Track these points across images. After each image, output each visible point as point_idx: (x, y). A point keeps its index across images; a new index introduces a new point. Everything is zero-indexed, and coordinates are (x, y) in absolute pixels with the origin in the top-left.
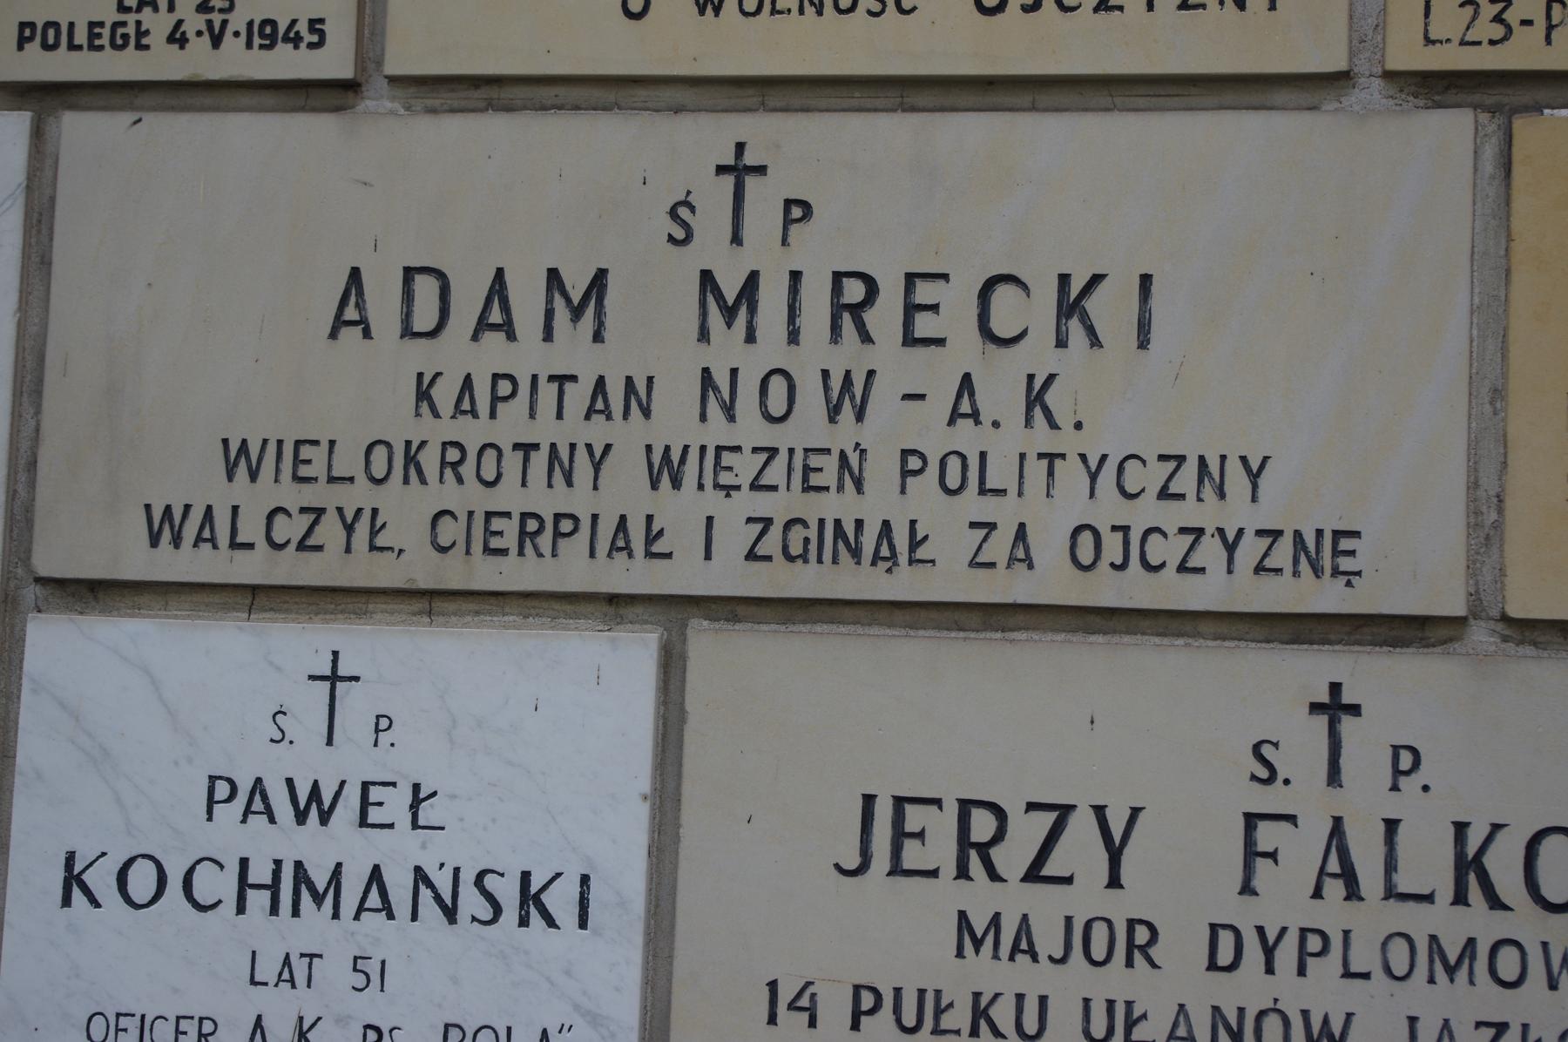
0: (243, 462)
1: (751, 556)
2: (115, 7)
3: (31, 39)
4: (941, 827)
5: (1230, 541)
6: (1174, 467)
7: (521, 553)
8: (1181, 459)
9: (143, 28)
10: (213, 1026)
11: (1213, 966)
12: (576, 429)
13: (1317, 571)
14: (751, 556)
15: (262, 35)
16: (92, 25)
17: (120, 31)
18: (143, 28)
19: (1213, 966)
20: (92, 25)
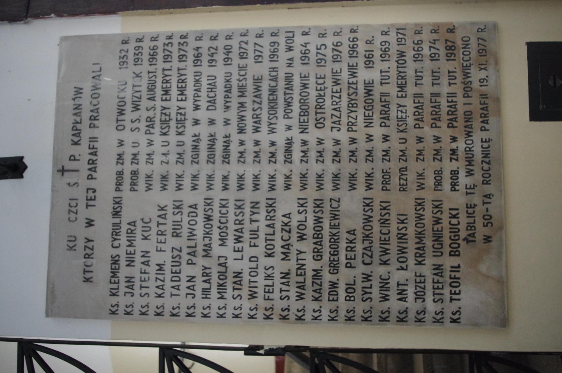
3: (119, 188)
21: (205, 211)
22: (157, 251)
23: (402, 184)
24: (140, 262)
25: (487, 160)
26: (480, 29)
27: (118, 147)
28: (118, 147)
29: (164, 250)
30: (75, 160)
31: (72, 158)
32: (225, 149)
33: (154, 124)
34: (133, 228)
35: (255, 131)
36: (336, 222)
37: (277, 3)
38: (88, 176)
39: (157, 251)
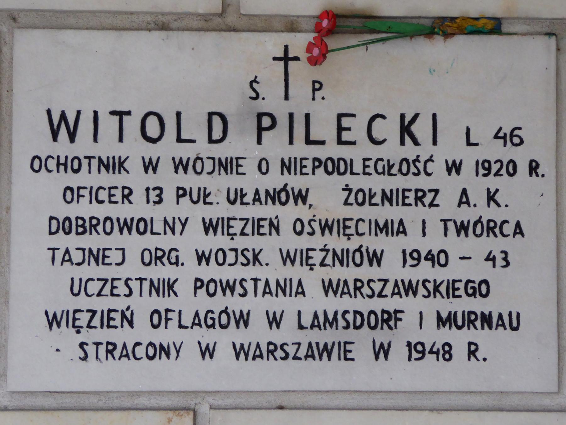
0: (63, 126)
1: (437, 191)
2: (211, 111)
3: (201, 287)
4: (412, 195)
5: (372, 194)
6: (349, 199)
7: (123, 203)
8: (247, 220)
9: (244, 193)
10: (221, 135)
11: (51, 233)
12: (238, 211)
13: (90, 251)
14: (437, 191)
15: (484, 168)
16: (365, 160)
17: (471, 285)
18: (244, 193)
19: (51, 233)
20: (365, 160)
21: (429, 296)
22: (340, 116)
23: (232, 223)
24: (233, 341)
25: (329, 261)
26: (477, 349)
27: (196, 250)
28: (196, 250)
29: (132, 201)
30: (314, 90)
31: (317, 86)
32: (107, 168)
33: (320, 329)
34: (117, 353)
35: (326, 284)
36: (265, 230)
37: (50, 125)
38: (319, 82)
39: (340, 116)
